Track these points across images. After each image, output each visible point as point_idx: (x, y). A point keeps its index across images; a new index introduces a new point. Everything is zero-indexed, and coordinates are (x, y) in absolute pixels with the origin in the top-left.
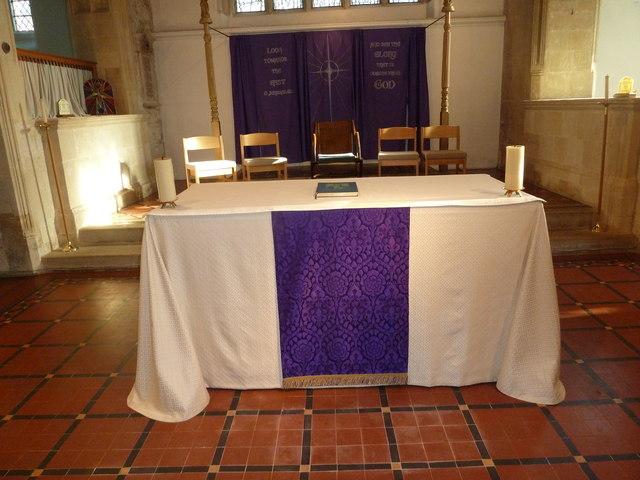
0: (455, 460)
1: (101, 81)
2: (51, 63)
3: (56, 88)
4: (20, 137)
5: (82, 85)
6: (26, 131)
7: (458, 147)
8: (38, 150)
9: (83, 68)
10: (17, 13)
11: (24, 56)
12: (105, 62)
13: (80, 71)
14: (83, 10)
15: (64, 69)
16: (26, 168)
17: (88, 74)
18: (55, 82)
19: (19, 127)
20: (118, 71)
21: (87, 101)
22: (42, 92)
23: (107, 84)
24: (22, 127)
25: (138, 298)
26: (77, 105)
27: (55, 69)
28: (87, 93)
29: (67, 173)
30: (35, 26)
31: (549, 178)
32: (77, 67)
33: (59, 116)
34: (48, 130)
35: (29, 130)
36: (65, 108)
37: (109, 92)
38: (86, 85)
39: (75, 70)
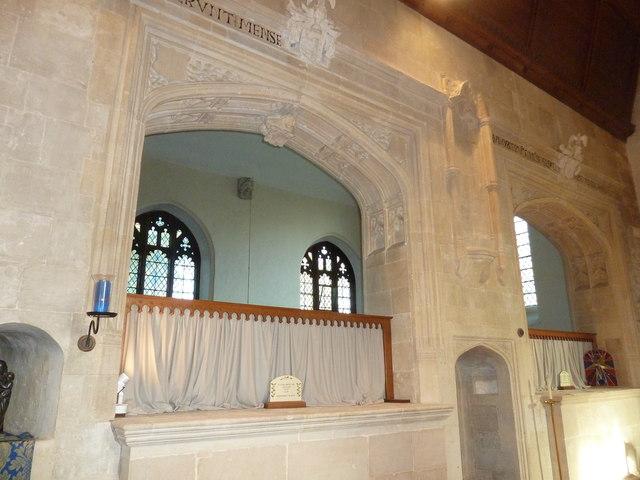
0: (136, 455)
1: (601, 351)
2: (555, 338)
3: (558, 362)
4: (527, 411)
5: (582, 356)
6: (533, 406)
7: (170, 291)
8: (542, 424)
9: (583, 340)
10: (148, 273)
11: (535, 334)
12: (605, 333)
13: (580, 343)
14: (583, 287)
15: (565, 343)
16: (531, 441)
17: (588, 346)
18: (558, 356)
19: (527, 401)
20: (618, 341)
21: (587, 372)
22: (546, 368)
23: (608, 355)
24: (529, 402)
25: (19, 333)
26: (577, 376)
27: (558, 343)
28: (587, 363)
29: (569, 450)
30: (538, 301)
31: (377, 334)
32: (578, 340)
33: (560, 388)
34: (552, 406)
35: (535, 405)
36: (566, 380)
37: (609, 362)
38: (586, 356)
39: (576, 342)
